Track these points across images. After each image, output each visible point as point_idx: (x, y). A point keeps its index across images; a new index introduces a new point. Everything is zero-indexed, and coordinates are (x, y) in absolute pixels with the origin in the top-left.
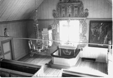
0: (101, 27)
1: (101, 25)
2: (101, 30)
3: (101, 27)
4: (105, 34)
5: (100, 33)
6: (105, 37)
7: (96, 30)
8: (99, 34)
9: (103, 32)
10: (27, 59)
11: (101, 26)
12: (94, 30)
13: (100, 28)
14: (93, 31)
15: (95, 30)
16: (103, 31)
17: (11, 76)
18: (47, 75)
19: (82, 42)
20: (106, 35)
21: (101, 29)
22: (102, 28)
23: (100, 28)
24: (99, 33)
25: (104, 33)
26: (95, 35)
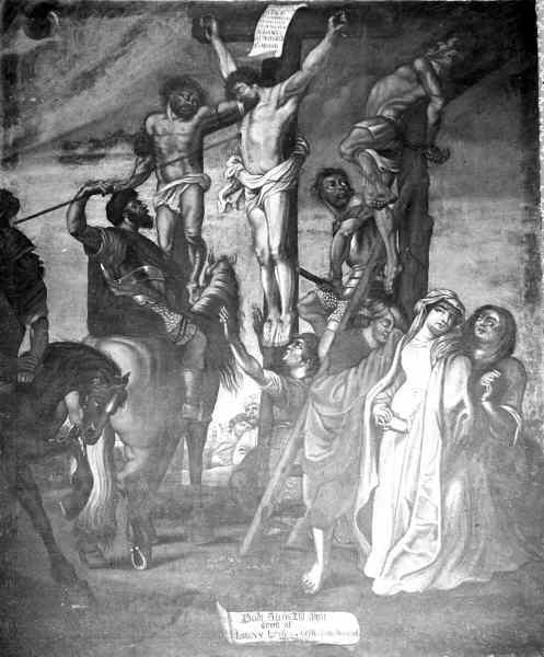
0: (264, 126)
1: (268, 73)
2: (275, 201)
3: (264, 126)
4: (377, 291)
5: (253, 291)
6: (302, 525)
7: (147, 194)
8: (232, 296)
9: (316, 255)
10: (485, 360)
11: (271, 95)
12: (97, 216)
13: (234, 148)
14: (61, 222)
15: (122, 200)
16: (315, 222)
17: (260, 492)
18: (340, 239)
19: (448, 504)
20: (405, 326)
21: (269, 175)
22: (288, 144)
23: (234, 148)
24: (230, 273)
25: (351, 281)
26: (141, 293)
